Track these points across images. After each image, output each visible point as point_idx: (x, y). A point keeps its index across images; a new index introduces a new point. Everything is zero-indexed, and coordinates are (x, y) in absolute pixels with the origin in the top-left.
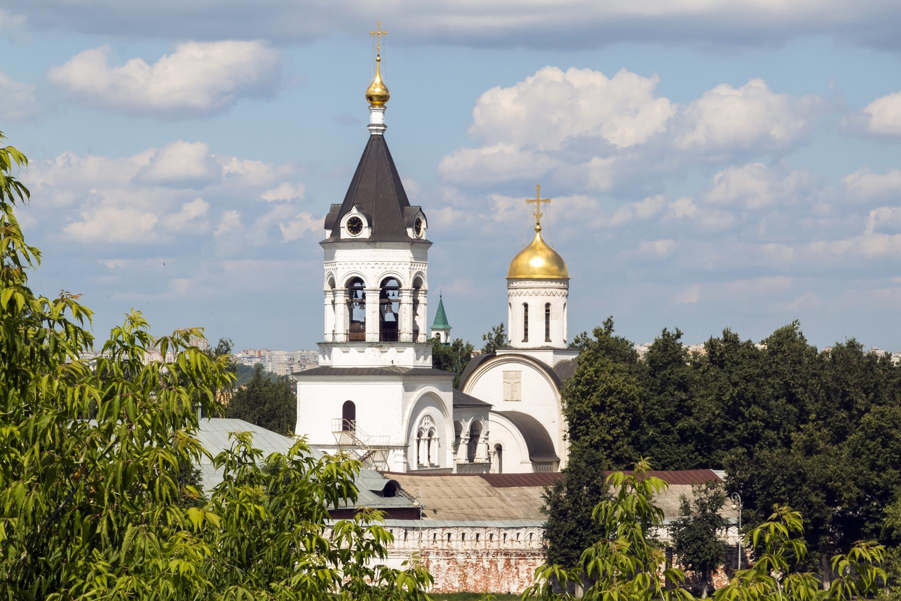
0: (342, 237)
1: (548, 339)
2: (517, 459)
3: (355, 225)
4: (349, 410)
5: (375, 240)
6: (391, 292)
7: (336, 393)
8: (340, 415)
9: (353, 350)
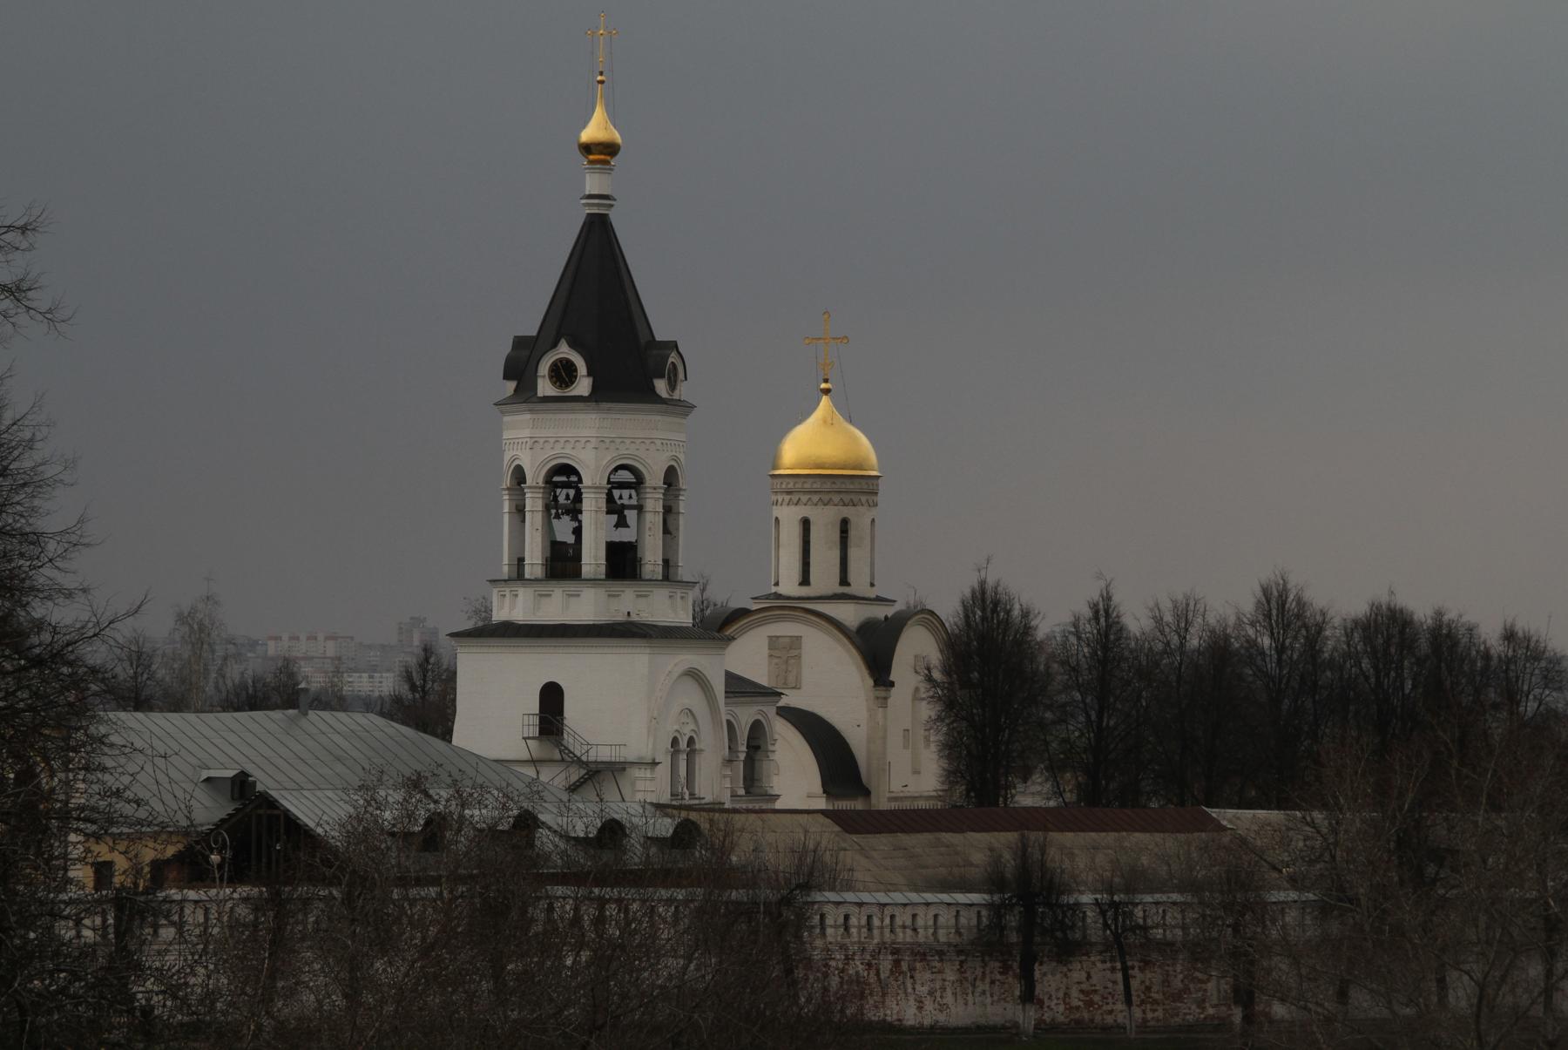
0: (540, 394)
1: (844, 581)
3: (562, 374)
4: (552, 697)
6: (616, 493)
7: (524, 671)
8: (535, 707)
9: (558, 591)
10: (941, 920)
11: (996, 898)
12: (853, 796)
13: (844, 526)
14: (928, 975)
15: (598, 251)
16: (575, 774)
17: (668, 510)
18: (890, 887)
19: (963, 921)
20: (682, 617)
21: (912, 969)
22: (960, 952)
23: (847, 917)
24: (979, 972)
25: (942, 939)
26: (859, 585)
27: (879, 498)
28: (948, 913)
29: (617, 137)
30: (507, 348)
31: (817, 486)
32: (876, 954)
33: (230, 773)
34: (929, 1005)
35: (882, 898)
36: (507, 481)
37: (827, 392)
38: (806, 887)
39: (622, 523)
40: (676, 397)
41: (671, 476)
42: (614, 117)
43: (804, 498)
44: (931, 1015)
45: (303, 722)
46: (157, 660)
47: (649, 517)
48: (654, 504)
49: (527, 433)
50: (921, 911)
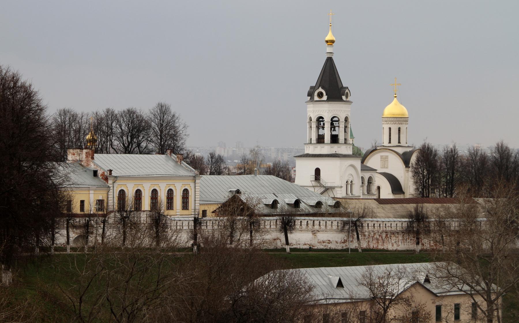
1: (399, 142)
2: (387, 193)
3: (320, 95)
4: (318, 171)
5: (329, 99)
6: (335, 123)
9: (319, 146)
10: (398, 225)
11: (410, 220)
12: (400, 194)
13: (399, 129)
14: (395, 238)
15: (330, 62)
16: (323, 189)
17: (346, 127)
18: (388, 217)
19: (403, 225)
20: (350, 152)
21: (391, 237)
22: (403, 233)
23: (374, 224)
24: (407, 237)
25: (398, 229)
26: (403, 143)
27: (408, 122)
28: (400, 223)
29: (334, 39)
30: (308, 89)
31: (393, 119)
32: (382, 233)
33: (235, 190)
34: (395, 245)
35: (383, 220)
36: (308, 120)
37: (396, 97)
38: (363, 217)
39: (334, 130)
40: (348, 100)
41: (346, 119)
42: (333, 34)
43: (390, 123)
44: (395, 247)
45: (256, 178)
46: (459, 164)
47: (341, 129)
48: (342, 125)
49: (312, 109)
50: (393, 223)
